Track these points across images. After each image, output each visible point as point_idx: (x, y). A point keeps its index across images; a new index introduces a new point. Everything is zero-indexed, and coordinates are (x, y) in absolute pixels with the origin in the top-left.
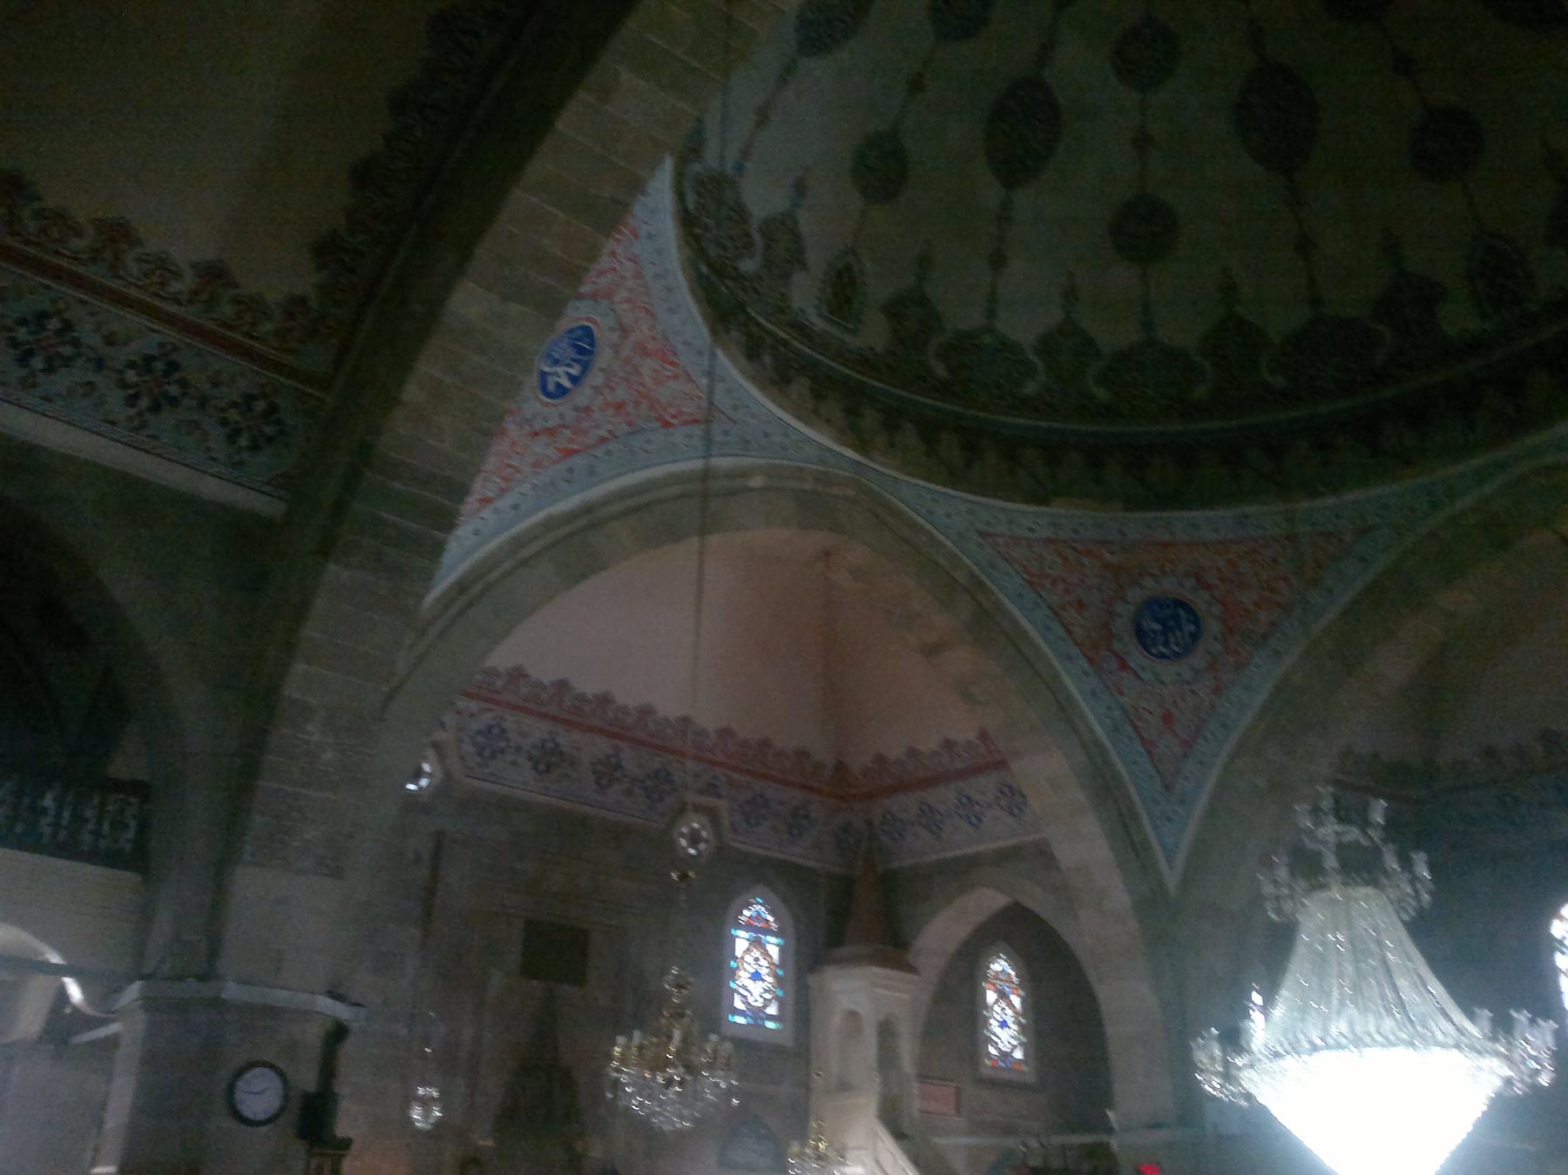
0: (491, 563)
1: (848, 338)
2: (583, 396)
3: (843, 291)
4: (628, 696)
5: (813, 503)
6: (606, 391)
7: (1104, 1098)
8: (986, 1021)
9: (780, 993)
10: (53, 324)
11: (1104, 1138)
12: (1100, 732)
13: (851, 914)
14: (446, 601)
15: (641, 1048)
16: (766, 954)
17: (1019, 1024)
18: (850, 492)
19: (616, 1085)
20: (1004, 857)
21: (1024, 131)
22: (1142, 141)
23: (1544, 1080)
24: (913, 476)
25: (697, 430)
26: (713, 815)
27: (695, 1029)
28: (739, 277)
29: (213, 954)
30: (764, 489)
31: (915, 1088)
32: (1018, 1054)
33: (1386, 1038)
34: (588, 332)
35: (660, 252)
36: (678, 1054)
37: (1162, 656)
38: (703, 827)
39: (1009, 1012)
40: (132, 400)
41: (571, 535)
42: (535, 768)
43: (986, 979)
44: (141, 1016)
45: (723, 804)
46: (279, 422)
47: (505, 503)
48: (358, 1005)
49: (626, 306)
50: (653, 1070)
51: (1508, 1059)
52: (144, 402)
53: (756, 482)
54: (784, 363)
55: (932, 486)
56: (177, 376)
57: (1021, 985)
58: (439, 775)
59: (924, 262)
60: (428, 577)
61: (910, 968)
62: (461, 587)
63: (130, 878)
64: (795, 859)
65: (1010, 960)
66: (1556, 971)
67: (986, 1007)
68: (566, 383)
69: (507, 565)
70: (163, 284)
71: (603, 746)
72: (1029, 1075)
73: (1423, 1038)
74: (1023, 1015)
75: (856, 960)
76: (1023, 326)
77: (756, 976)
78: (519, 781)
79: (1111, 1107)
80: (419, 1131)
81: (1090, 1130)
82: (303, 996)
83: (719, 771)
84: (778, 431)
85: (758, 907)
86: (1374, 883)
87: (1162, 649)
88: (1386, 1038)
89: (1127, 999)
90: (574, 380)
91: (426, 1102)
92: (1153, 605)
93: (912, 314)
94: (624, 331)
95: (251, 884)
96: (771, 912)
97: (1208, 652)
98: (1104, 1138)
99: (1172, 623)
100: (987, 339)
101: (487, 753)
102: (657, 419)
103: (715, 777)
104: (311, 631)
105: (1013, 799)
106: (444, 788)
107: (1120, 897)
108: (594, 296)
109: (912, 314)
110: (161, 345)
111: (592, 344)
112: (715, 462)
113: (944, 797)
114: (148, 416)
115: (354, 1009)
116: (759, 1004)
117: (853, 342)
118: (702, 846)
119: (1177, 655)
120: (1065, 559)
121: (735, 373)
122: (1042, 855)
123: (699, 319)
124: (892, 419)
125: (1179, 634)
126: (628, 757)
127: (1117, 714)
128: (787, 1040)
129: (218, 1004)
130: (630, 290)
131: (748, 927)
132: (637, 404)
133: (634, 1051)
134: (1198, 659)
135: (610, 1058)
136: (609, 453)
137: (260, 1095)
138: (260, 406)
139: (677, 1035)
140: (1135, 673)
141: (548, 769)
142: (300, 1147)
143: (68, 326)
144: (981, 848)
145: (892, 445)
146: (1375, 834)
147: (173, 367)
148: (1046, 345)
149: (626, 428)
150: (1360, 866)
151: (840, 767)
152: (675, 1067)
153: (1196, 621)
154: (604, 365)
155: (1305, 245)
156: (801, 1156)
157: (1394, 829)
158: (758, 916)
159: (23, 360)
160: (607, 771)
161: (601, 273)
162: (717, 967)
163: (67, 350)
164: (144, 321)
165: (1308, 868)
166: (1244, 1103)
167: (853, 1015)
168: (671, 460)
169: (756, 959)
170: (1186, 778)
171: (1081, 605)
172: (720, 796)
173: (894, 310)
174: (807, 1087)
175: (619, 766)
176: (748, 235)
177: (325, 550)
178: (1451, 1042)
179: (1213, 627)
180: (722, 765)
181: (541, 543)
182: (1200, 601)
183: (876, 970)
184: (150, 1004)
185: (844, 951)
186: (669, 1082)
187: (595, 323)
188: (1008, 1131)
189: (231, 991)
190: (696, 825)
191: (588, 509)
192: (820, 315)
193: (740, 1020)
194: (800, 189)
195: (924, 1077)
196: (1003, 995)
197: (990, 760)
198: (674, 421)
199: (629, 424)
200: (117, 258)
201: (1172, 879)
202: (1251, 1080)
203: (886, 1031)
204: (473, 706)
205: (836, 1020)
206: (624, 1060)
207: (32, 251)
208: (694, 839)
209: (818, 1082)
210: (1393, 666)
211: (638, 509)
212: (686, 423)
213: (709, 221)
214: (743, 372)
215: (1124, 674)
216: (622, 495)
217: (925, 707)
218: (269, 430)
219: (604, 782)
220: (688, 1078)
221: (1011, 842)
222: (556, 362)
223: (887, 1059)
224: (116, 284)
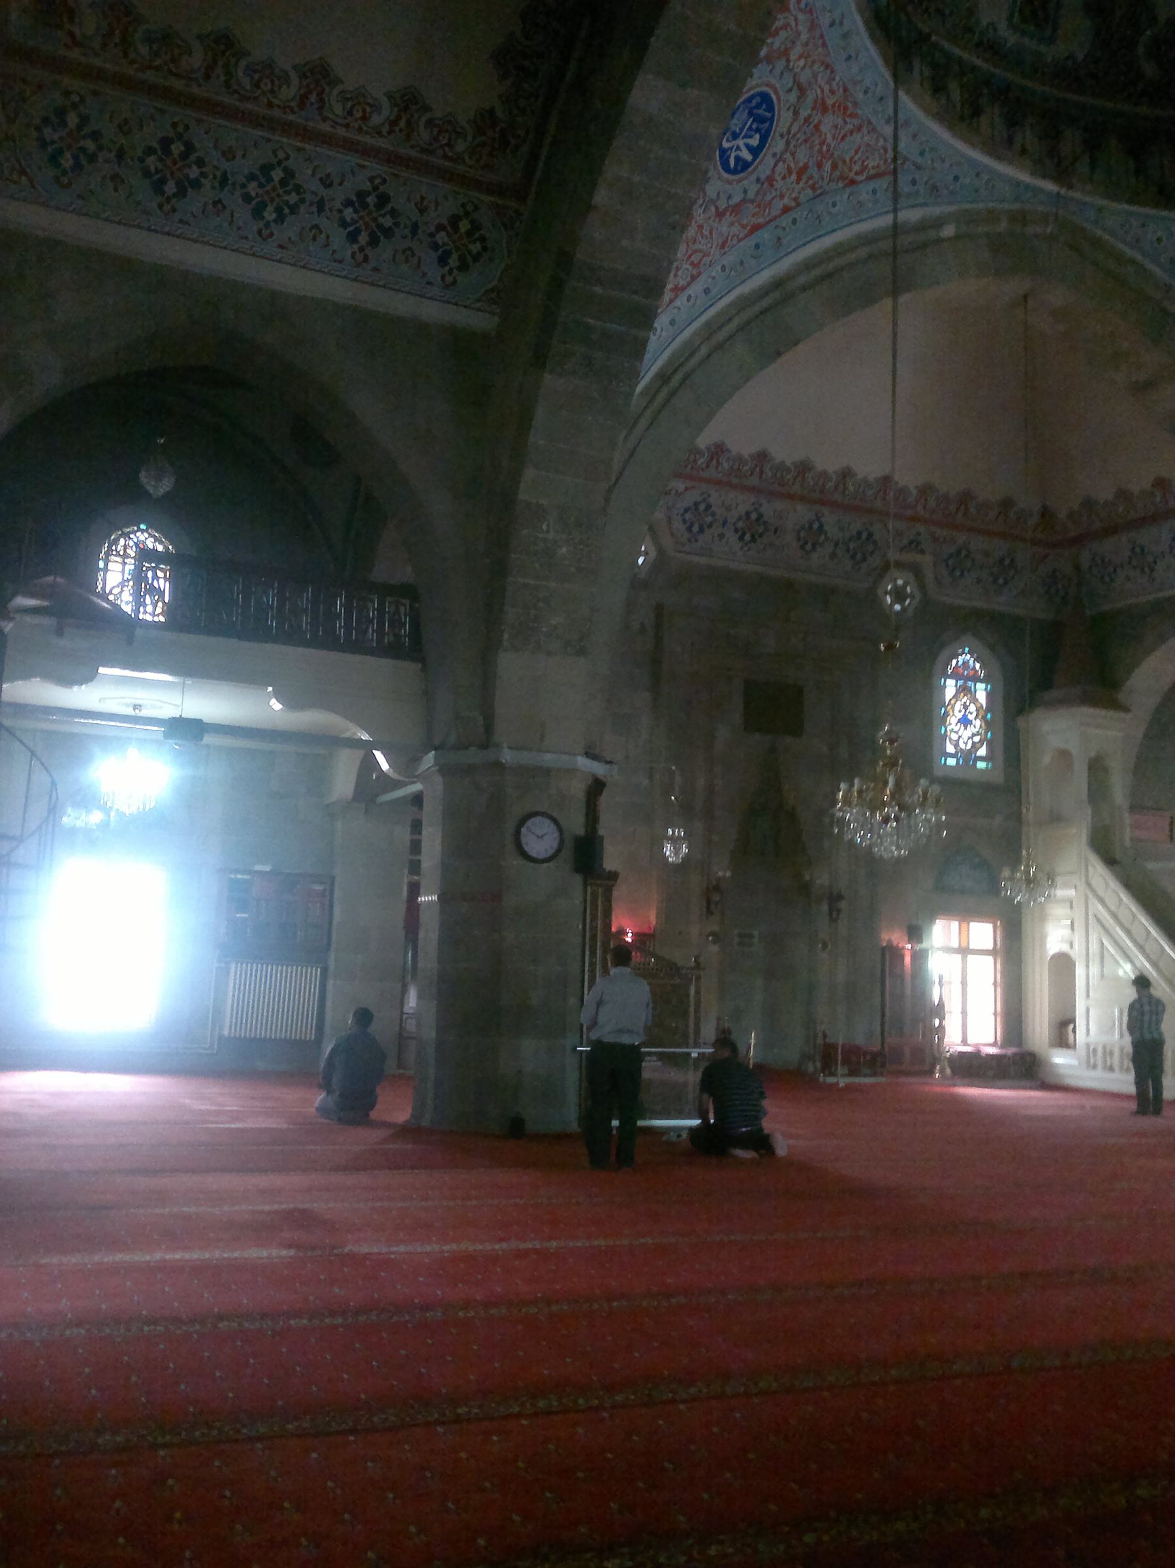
0: (689, 350)
1: (1043, 48)
4: (828, 462)
5: (1010, 245)
10: (277, 175)
14: (651, 392)
15: (860, 792)
16: (974, 700)
19: (841, 822)
25: (884, 183)
26: (916, 571)
27: (907, 772)
29: (489, 729)
30: (957, 237)
31: (1128, 819)
34: (765, 98)
36: (893, 796)
40: (353, 237)
41: (764, 312)
44: (438, 779)
46: (483, 239)
47: (696, 288)
48: (610, 762)
49: (802, 63)
52: (363, 238)
53: (949, 231)
56: (388, 208)
58: (653, 554)
60: (635, 375)
61: (1126, 710)
62: (663, 378)
63: (412, 667)
68: (746, 155)
69: (704, 351)
70: (364, 118)
71: (801, 513)
77: (965, 721)
78: (728, 552)
80: (673, 864)
82: (566, 757)
83: (922, 528)
84: (969, 171)
91: (674, 840)
95: (511, 666)
101: (695, 529)
103: (919, 534)
104: (537, 439)
106: (660, 562)
110: (371, 179)
111: (771, 108)
112: (903, 216)
114: (369, 251)
115: (607, 766)
121: (920, 114)
123: (880, 62)
126: (830, 520)
128: (999, 778)
129: (498, 766)
131: (956, 675)
132: (820, 165)
137: (541, 839)
138: (464, 226)
141: (753, 539)
142: (578, 879)
143: (289, 174)
147: (383, 199)
152: (890, 806)
156: (1012, 879)
158: (965, 663)
159: (258, 213)
160: (811, 536)
162: (926, 716)
163: (293, 198)
164: (354, 159)
167: (1064, 754)
168: (857, 219)
172: (922, 552)
174: (1018, 818)
177: (540, 358)
181: (736, 322)
184: (445, 770)
186: (886, 820)
189: (507, 756)
191: (777, 284)
193: (951, 762)
198: (859, 178)
200: (322, 100)
203: (1097, 768)
204: (680, 485)
205: (1047, 759)
206: (847, 801)
207: (249, 106)
208: (899, 595)
211: (830, 275)
212: (870, 178)
214: (926, 110)
216: (808, 265)
218: (476, 247)
222: (735, 136)
223: (1097, 792)
224: (326, 127)
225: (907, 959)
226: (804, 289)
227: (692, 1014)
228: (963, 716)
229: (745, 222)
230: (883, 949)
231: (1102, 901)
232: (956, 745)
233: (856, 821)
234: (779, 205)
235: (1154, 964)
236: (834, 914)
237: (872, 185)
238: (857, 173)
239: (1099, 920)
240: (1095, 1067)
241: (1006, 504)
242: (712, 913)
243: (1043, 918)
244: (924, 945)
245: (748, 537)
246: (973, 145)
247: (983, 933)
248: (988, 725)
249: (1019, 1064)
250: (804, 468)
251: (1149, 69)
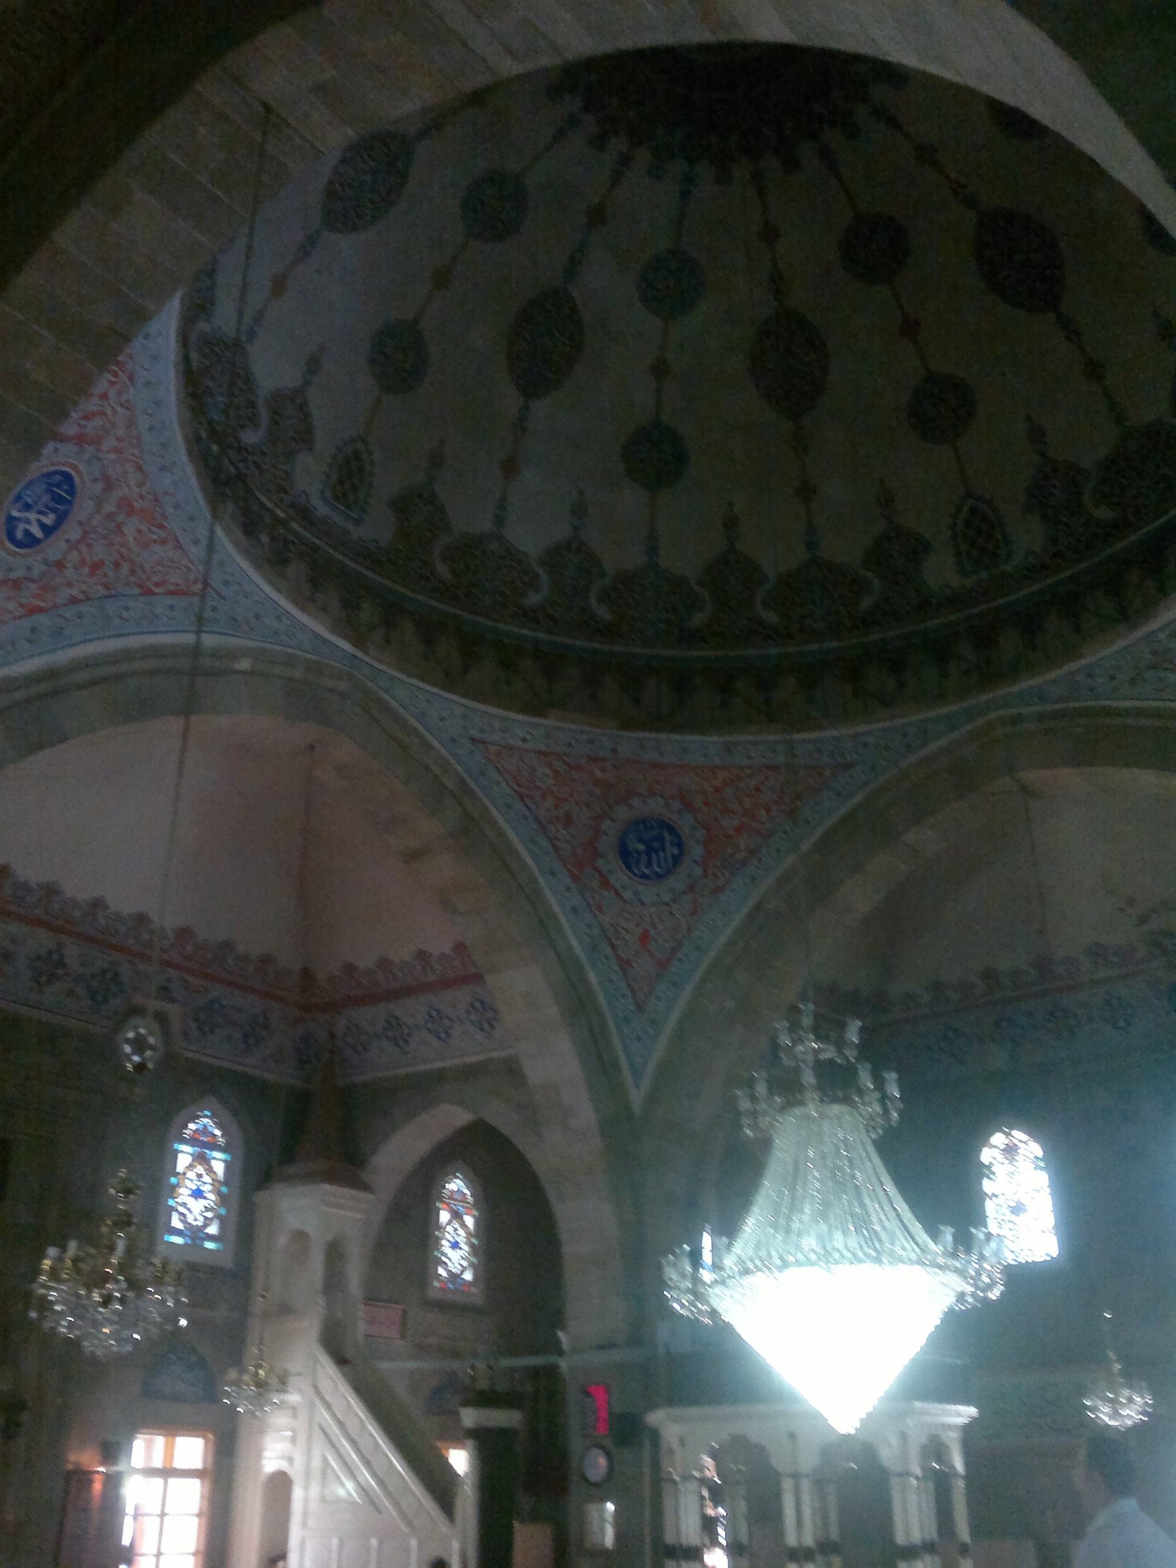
1: (351, 528)
2: (55, 549)
3: (349, 477)
4: (77, 887)
6: (82, 547)
7: (557, 1319)
8: (438, 1239)
9: (223, 1211)
11: (553, 1359)
12: (578, 949)
13: (306, 1125)
15: (76, 1260)
16: (210, 1170)
17: (471, 1245)
18: (343, 686)
19: (44, 1305)
20: (469, 1073)
21: (547, 338)
22: (660, 370)
23: (994, 1294)
24: (410, 675)
26: (161, 1018)
28: (241, 449)
31: (361, 1311)
32: (468, 1276)
33: (854, 1255)
34: (68, 478)
35: (158, 403)
36: (121, 1269)
37: (644, 876)
38: (151, 1034)
39: (461, 1232)
43: (440, 1198)
45: (173, 1010)
49: (113, 456)
50: (89, 1289)
51: (961, 1273)
53: (244, 665)
54: (283, 542)
55: (428, 688)
57: (476, 1205)
59: (436, 461)
61: (367, 1188)
64: (250, 1071)
65: (466, 1179)
66: (983, 1196)
67: (440, 1228)
68: (37, 532)
71: (42, 941)
72: (477, 1297)
73: (891, 1254)
74: (476, 1236)
75: (311, 1177)
76: (532, 534)
77: (198, 1194)
79: (563, 1329)
81: (534, 1351)
83: (173, 973)
84: (269, 613)
85: (206, 1120)
86: (846, 1100)
87: (647, 871)
88: (854, 1255)
89: (585, 1220)
90: (48, 530)
92: (641, 822)
93: (417, 509)
94: (109, 484)
96: (219, 1125)
97: (689, 875)
98: (553, 1359)
99: (656, 845)
100: (494, 546)
102: (139, 586)
103: (169, 980)
105: (486, 1014)
107: (585, 1114)
108: (80, 440)
109: (417, 509)
111: (72, 491)
113: (412, 1010)
116: (200, 1223)
117: (356, 532)
118: (148, 1053)
119: (659, 876)
120: (557, 772)
122: (512, 1070)
124: (392, 613)
125: (661, 854)
126: (72, 952)
127: (596, 931)
128: (227, 1262)
130: (120, 440)
131: (193, 1141)
132: (117, 565)
133: (69, 1263)
134: (678, 882)
135: (37, 1271)
136: (80, 616)
139: (121, 1246)
140: (617, 893)
144: (447, 1064)
145: (388, 641)
146: (851, 1054)
148: (553, 558)
149: (102, 591)
150: (836, 1083)
151: (306, 973)
152: (117, 1282)
153: (680, 845)
154: (83, 519)
155: (806, 491)
156: (237, 1383)
157: (866, 1050)
160: (48, 969)
161: (88, 417)
162: (156, 1183)
165: (788, 1089)
166: (707, 1321)
167: (300, 1236)
169: (200, 1176)
170: (658, 998)
171: (568, 820)
172: (172, 1000)
173: (402, 505)
175: (61, 964)
176: (252, 404)
178: (913, 1256)
179: (696, 851)
180: (177, 967)
182: (685, 824)
183: (327, 1187)
185: (292, 1169)
186: (107, 1301)
187: (76, 469)
188: (456, 1354)
190: (142, 1031)
191: (52, 673)
192: (324, 499)
194: (313, 364)
195: (370, 1299)
196: (456, 1216)
197: (463, 973)
199: (107, 587)
201: (637, 1097)
202: (717, 1295)
203: (335, 1253)
205: (282, 1241)
206: (54, 1274)
208: (139, 1045)
209: (258, 1304)
210: (859, 897)
212: (171, 593)
213: (213, 375)
214: (236, 544)
215: (605, 893)
216: (86, 664)
217: (399, 918)
219: (43, 979)
220: (130, 1294)
221: (481, 1057)
222: (27, 507)
223: (333, 1281)
225: (97, 1486)
226: (81, 687)
228: (196, 1188)
229: (24, 601)
230: (69, 1475)
231: (328, 1406)
233: (64, 1302)
234: (66, 593)
235: (381, 1482)
237: (170, 600)
238: (157, 584)
239: (323, 1430)
243: (262, 1430)
244: (121, 1467)
246: (278, 590)
247: (191, 1450)
248: (223, 1199)
251: (442, 569)
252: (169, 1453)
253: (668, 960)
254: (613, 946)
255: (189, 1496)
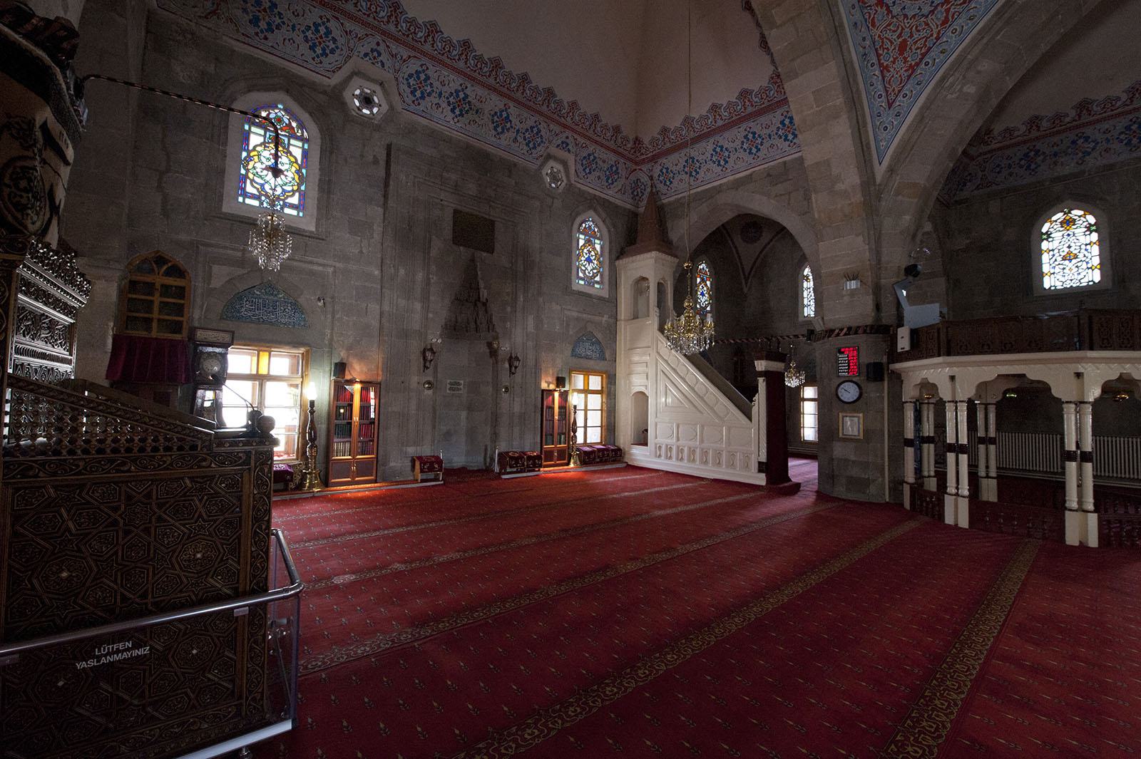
16: (594, 249)
42: (453, 111)
158: (590, 227)
162: (567, 252)
175: (507, 119)
203: (661, 288)
227: (614, 466)
228: (588, 256)
232: (584, 273)
236: (512, 370)
240: (682, 459)
241: (617, 129)
242: (428, 368)
245: (457, 112)
247: (595, 382)
249: (608, 455)
250: (497, 64)
252: (587, 382)
253: (918, 64)
254: (878, 56)
255: (595, 401)
